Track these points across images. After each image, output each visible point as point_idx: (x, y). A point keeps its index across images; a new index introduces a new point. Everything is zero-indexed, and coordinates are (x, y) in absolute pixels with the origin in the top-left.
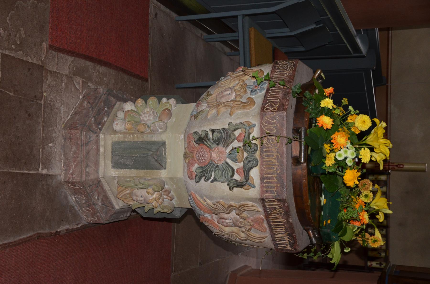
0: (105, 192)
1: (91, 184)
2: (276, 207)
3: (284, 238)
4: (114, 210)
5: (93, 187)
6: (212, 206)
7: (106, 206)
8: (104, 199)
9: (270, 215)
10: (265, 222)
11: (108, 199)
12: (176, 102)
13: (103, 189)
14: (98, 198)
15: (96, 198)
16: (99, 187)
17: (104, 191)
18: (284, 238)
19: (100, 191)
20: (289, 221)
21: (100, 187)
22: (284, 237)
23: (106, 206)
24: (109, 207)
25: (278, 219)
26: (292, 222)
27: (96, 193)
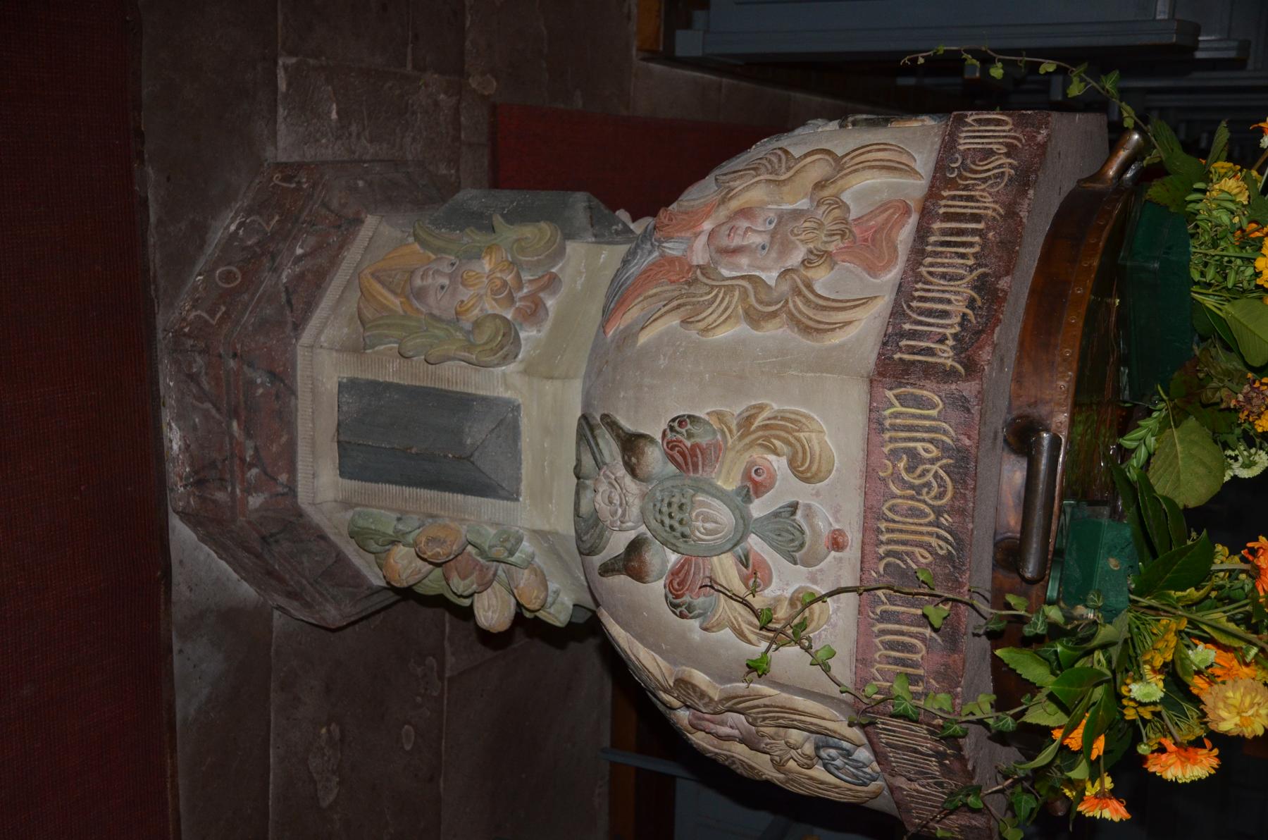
0: (334, 261)
1: (332, 208)
2: (994, 147)
3: (949, 302)
4: (292, 334)
5: (326, 218)
6: (590, 455)
7: (289, 302)
8: (309, 276)
9: (952, 184)
10: (913, 219)
11: (319, 286)
12: (484, 628)
13: (341, 248)
14: (300, 258)
15: (299, 251)
16: (340, 233)
17: (338, 255)
18: (949, 302)
19: (329, 244)
20: (1017, 215)
21: (343, 234)
22: (953, 298)
23: (289, 302)
24: (292, 311)
25: (1001, 140)
26: (1025, 220)
27: (312, 241)
